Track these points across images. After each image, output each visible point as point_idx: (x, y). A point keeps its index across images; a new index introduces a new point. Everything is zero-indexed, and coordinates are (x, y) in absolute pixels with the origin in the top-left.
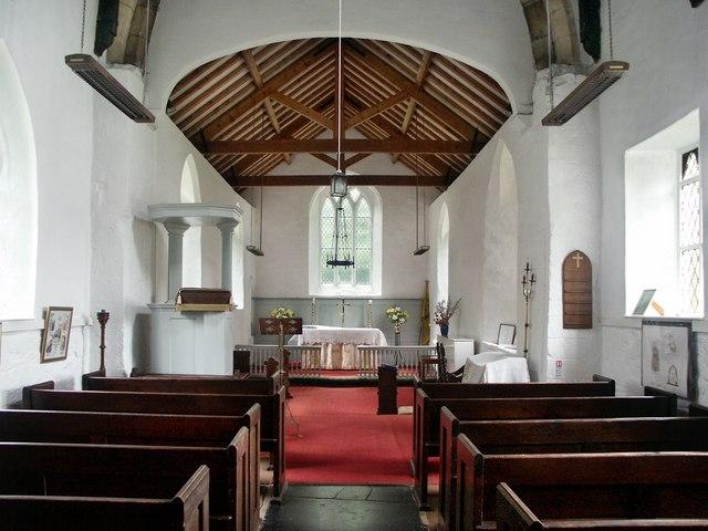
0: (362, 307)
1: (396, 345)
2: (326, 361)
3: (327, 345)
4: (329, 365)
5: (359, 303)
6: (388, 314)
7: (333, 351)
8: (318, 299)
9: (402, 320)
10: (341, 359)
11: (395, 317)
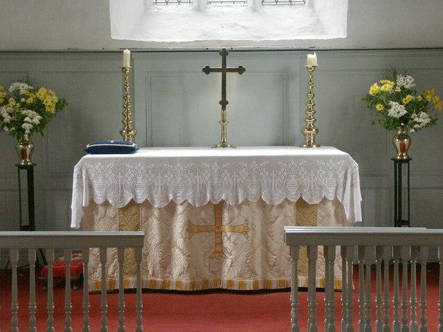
0: (284, 78)
1: (399, 223)
2: (166, 262)
3: (171, 208)
4: (179, 274)
5: (274, 63)
6: (373, 100)
7: (190, 229)
8: (145, 53)
9: (423, 118)
10: (219, 253)
11: (397, 110)
